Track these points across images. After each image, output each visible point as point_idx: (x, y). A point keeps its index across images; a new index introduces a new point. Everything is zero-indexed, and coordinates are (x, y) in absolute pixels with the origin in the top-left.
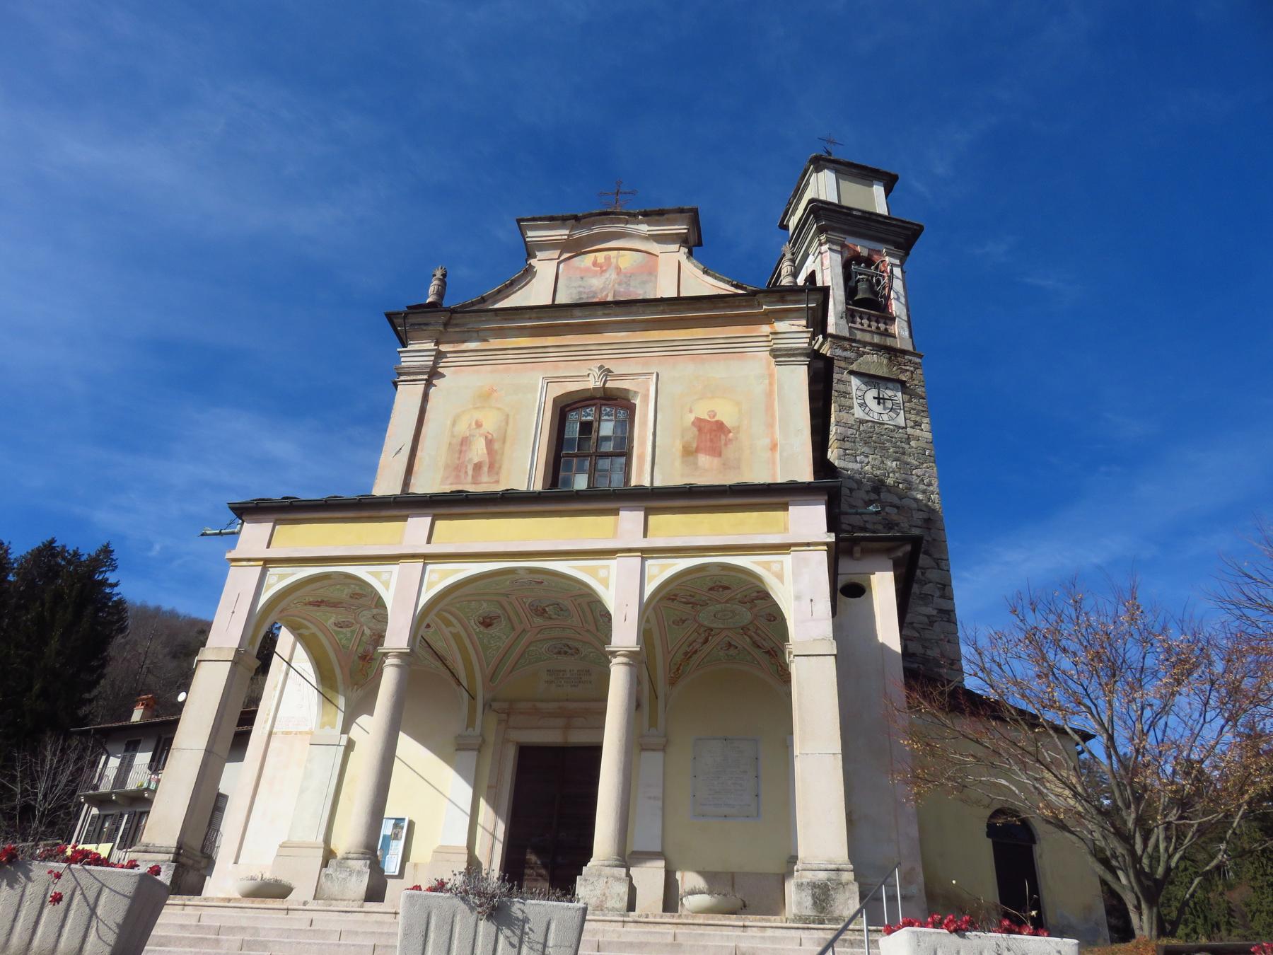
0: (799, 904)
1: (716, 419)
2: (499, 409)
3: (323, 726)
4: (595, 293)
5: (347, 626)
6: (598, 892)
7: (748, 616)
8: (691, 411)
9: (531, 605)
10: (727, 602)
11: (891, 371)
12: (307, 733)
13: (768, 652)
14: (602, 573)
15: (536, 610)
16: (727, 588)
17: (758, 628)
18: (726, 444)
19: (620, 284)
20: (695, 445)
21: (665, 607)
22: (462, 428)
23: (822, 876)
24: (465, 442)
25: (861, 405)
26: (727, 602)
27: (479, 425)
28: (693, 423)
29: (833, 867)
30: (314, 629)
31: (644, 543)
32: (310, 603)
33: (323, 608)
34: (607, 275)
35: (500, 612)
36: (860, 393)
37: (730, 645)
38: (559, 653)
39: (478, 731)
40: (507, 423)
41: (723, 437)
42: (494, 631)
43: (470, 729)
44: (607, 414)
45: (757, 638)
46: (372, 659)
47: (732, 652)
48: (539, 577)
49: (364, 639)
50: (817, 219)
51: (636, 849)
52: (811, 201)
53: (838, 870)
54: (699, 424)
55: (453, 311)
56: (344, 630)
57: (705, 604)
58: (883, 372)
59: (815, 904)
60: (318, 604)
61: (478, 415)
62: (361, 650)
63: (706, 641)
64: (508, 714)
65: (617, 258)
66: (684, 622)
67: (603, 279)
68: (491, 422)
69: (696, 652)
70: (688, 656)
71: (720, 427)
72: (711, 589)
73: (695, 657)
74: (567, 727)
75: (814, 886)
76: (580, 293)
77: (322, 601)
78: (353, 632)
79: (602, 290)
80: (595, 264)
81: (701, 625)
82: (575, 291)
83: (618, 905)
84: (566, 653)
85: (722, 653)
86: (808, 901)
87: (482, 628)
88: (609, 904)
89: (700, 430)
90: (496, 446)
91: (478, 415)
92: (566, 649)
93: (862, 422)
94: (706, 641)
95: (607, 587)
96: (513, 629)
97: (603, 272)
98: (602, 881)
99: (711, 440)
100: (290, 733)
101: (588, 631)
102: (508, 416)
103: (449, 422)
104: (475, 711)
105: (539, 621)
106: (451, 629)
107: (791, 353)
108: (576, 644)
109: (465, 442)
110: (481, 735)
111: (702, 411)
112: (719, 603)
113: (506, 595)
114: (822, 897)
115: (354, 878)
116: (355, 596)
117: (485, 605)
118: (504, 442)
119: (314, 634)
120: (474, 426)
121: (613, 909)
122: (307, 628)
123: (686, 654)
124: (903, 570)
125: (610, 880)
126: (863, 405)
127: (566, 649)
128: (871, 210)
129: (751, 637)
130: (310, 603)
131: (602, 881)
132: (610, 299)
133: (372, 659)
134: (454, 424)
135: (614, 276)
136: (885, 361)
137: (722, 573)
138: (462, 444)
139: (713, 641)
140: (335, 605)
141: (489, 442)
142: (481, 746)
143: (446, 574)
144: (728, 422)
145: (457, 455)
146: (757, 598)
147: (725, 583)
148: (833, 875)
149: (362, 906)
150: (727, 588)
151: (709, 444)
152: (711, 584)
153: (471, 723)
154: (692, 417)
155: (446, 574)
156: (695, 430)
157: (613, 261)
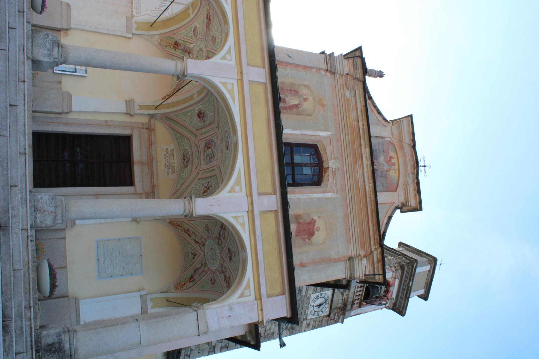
0: (48, 335)
1: (316, 231)
2: (314, 111)
3: (137, 23)
4: (377, 159)
5: (194, 34)
6: (46, 207)
7: (213, 267)
8: (319, 217)
9: (212, 141)
10: (221, 257)
11: (334, 309)
12: (132, 14)
13: (192, 277)
14: (237, 188)
15: (209, 143)
16: (231, 259)
17: (206, 272)
18: (302, 238)
19: (382, 172)
20: (301, 221)
21: (220, 232)
22: (304, 91)
23: (67, 347)
24: (296, 93)
25: (317, 296)
26: (221, 257)
27: (306, 100)
28: (313, 219)
29: (73, 352)
30: (192, 16)
31: (256, 212)
32: (209, 13)
33: (206, 20)
34: (386, 165)
35: (207, 123)
36: (323, 295)
37: (195, 255)
38: (184, 156)
39: (137, 112)
40: (307, 115)
41: (306, 236)
42: (196, 119)
43: (138, 107)
44: (314, 170)
45: (200, 271)
46: (176, 48)
47: (191, 256)
48: (232, 147)
49: (188, 44)
50: (408, 264)
51: (88, 320)
52: (416, 261)
53: (71, 356)
54: (312, 222)
55: (364, 83)
56: (192, 32)
57: (219, 245)
58: (334, 305)
59: (49, 345)
60: (208, 18)
61: (311, 99)
62: (181, 42)
63: (196, 242)
64: (147, 128)
65: (395, 169)
66: (208, 231)
67: (384, 163)
68: (307, 106)
69: (190, 236)
70: (187, 231)
71: (311, 234)
72: (229, 250)
73: (187, 235)
74: (142, 163)
75: (60, 342)
76: (376, 150)
77: (210, 20)
78: (191, 37)
79: (379, 163)
80: (391, 157)
81: (206, 240)
82: (377, 147)
83: (38, 221)
84: (184, 160)
85: (189, 250)
86: (50, 341)
87: (197, 112)
88: (39, 215)
89: (309, 223)
90: (295, 110)
91: (311, 99)
92: (186, 160)
93: (309, 298)
94: (196, 242)
95: (230, 192)
96: (197, 130)
97: (387, 162)
98: (52, 209)
99: (304, 230)
100: (132, 5)
101: (198, 173)
102: (311, 115)
103: (306, 83)
104: (148, 109)
105: (202, 145)
106: (195, 96)
107: (352, 269)
108: (189, 166)
109: (296, 93)
110: (136, 114)
111: (320, 223)
112: (221, 252)
113: (218, 127)
114: (53, 349)
115: (46, 52)
116: (214, 39)
117: (212, 114)
118: (297, 114)
119: (189, 15)
120: (304, 97)
121: (35, 217)
122: (193, 13)
123: (188, 230)
124: (239, 338)
125: (54, 214)
126: (317, 297)
127: (186, 160)
128: (412, 290)
129: (200, 268)
130: (209, 13)
131: (52, 209)
132: (375, 167)
133: (176, 48)
134: (306, 86)
135: (385, 168)
136: (339, 306)
137: (241, 260)
138: (295, 91)
139: (197, 246)
140: (208, 27)
141: (296, 106)
142: (129, 114)
143: (231, 93)
144: (315, 238)
145: (289, 88)
146: (225, 276)
147: (234, 259)
148: (68, 353)
149: (28, 58)
150: (231, 259)
151: (302, 229)
152: (233, 250)
153: (141, 107)
154: (316, 218)
155: (231, 93)
156: (309, 221)
157: (393, 167)
